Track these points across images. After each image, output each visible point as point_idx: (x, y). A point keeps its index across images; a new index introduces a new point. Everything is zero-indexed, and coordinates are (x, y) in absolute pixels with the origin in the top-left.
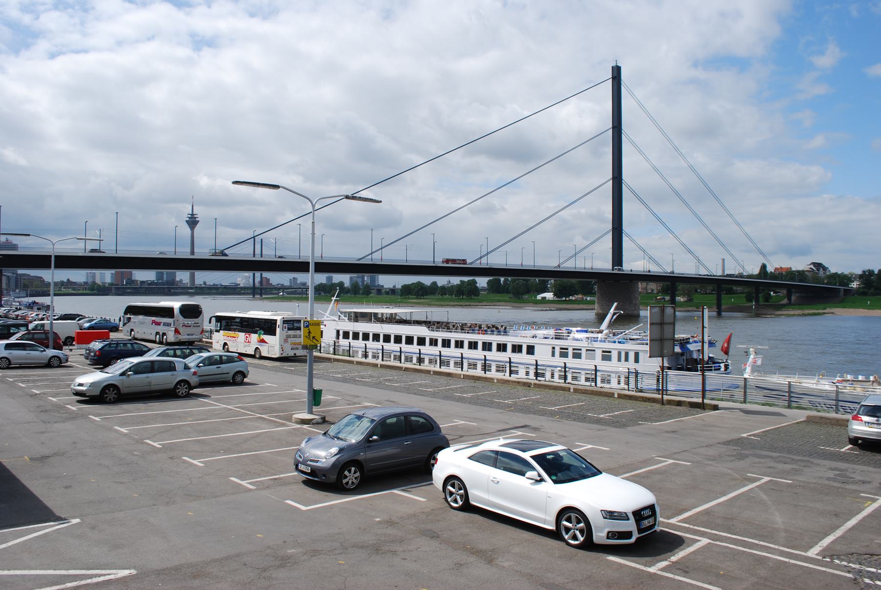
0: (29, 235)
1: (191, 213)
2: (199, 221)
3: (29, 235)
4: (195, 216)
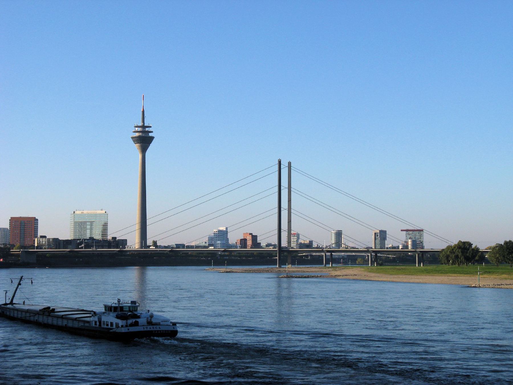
1: (141, 124)
4: (147, 129)
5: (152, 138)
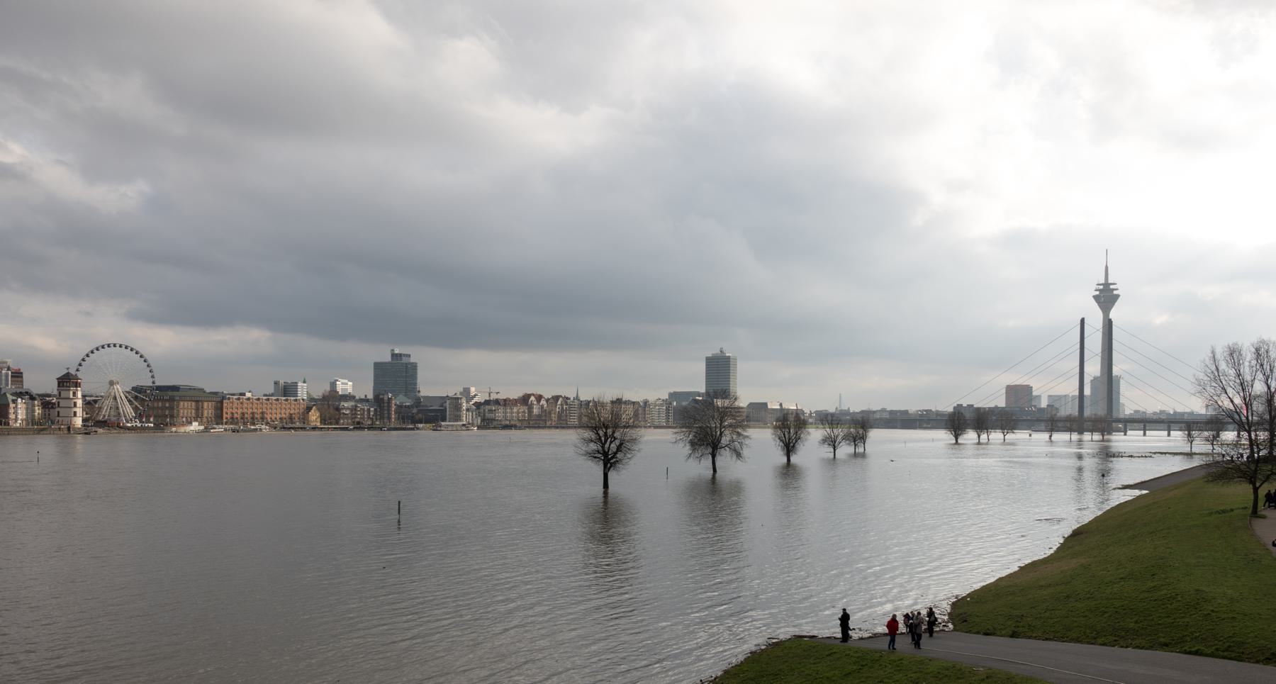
0: (1107, 268)
1: (1103, 282)
3: (1107, 268)
4: (1112, 287)
5: (1118, 296)
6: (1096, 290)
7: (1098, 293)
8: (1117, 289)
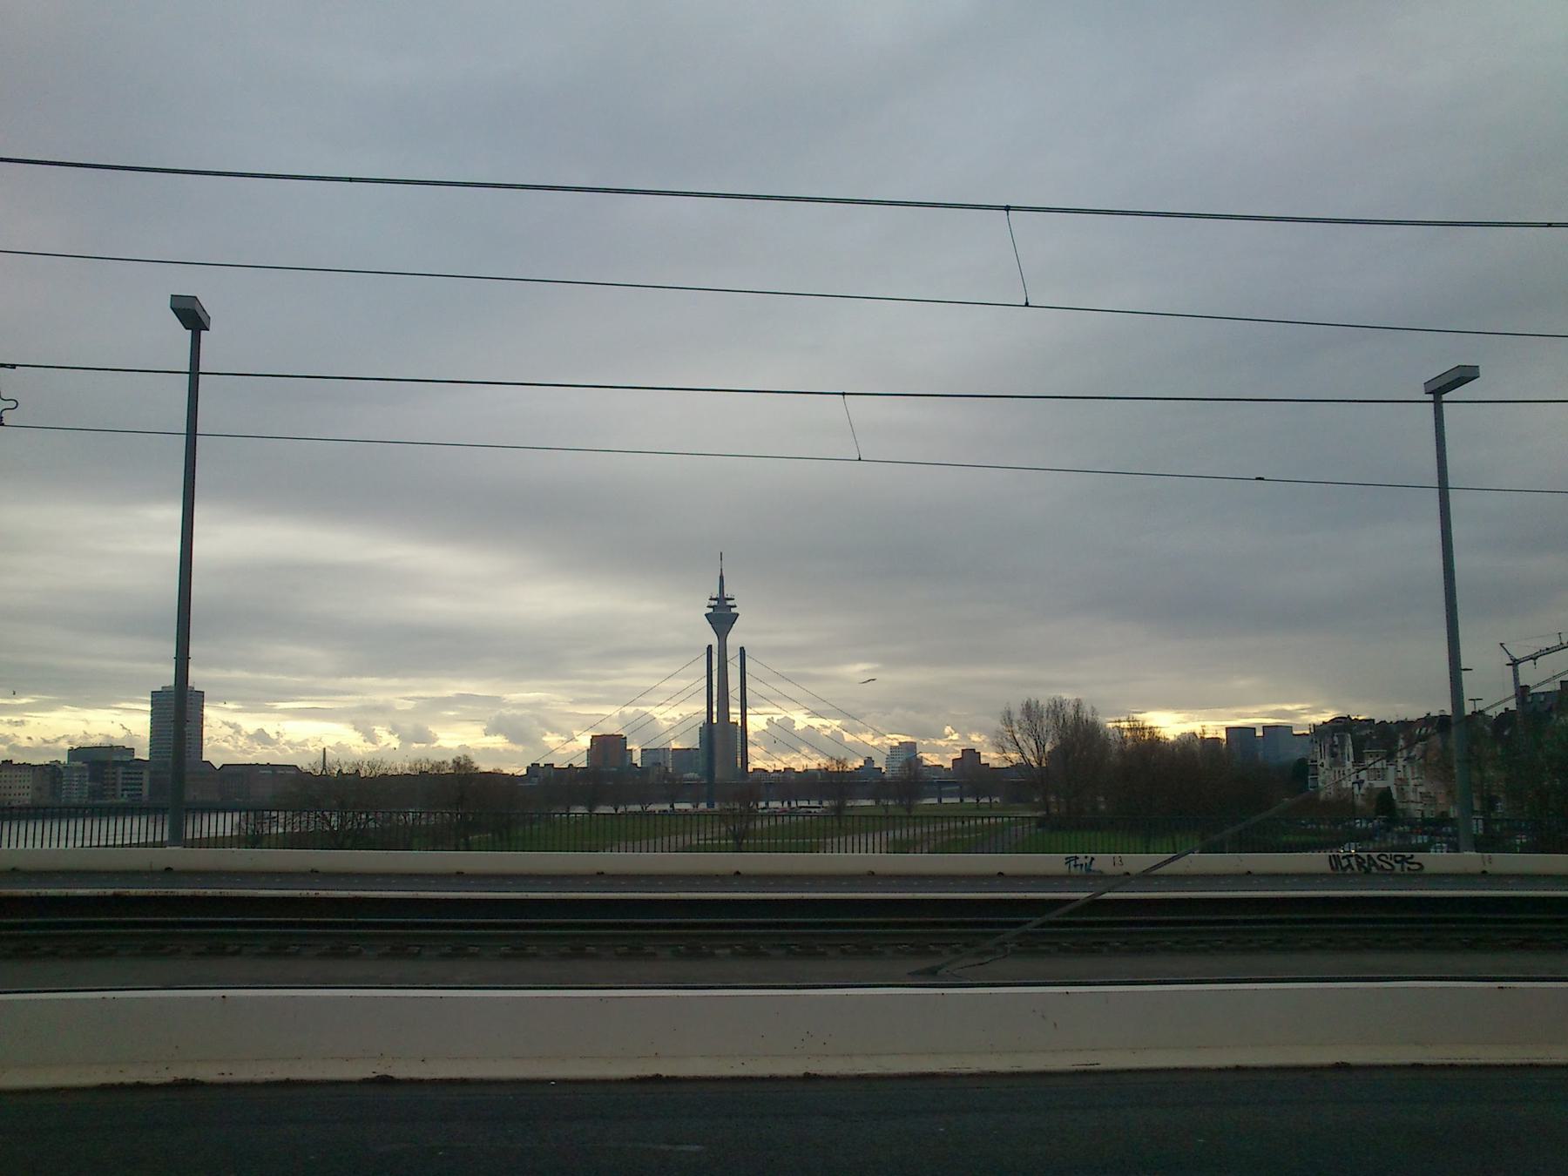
0: (721, 578)
2: (738, 615)
3: (721, 578)
4: (729, 603)
6: (709, 607)
7: (711, 610)
8: (735, 606)
